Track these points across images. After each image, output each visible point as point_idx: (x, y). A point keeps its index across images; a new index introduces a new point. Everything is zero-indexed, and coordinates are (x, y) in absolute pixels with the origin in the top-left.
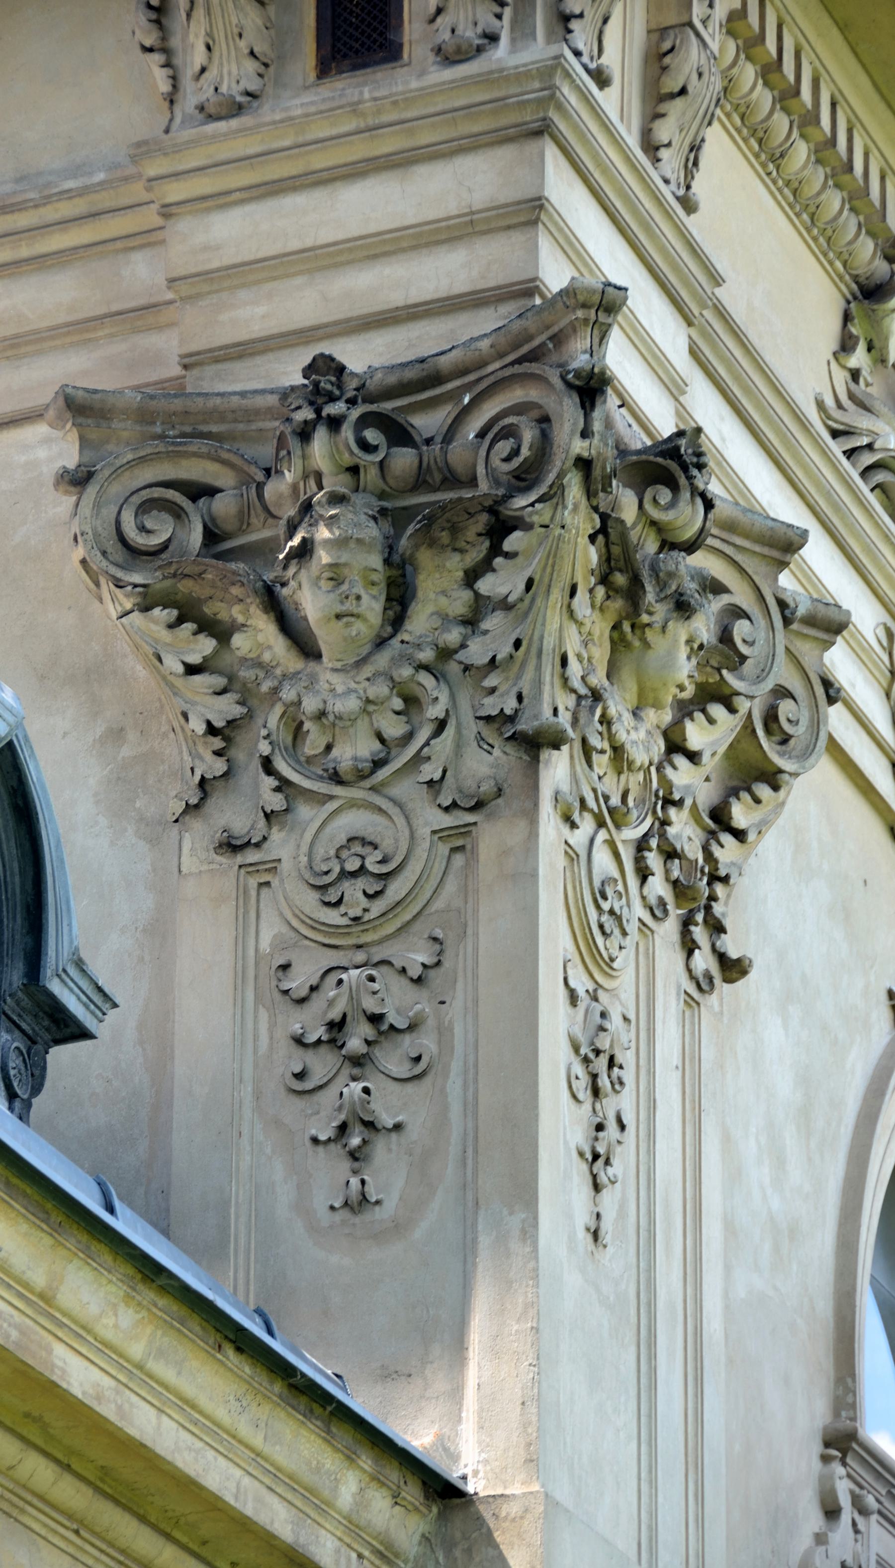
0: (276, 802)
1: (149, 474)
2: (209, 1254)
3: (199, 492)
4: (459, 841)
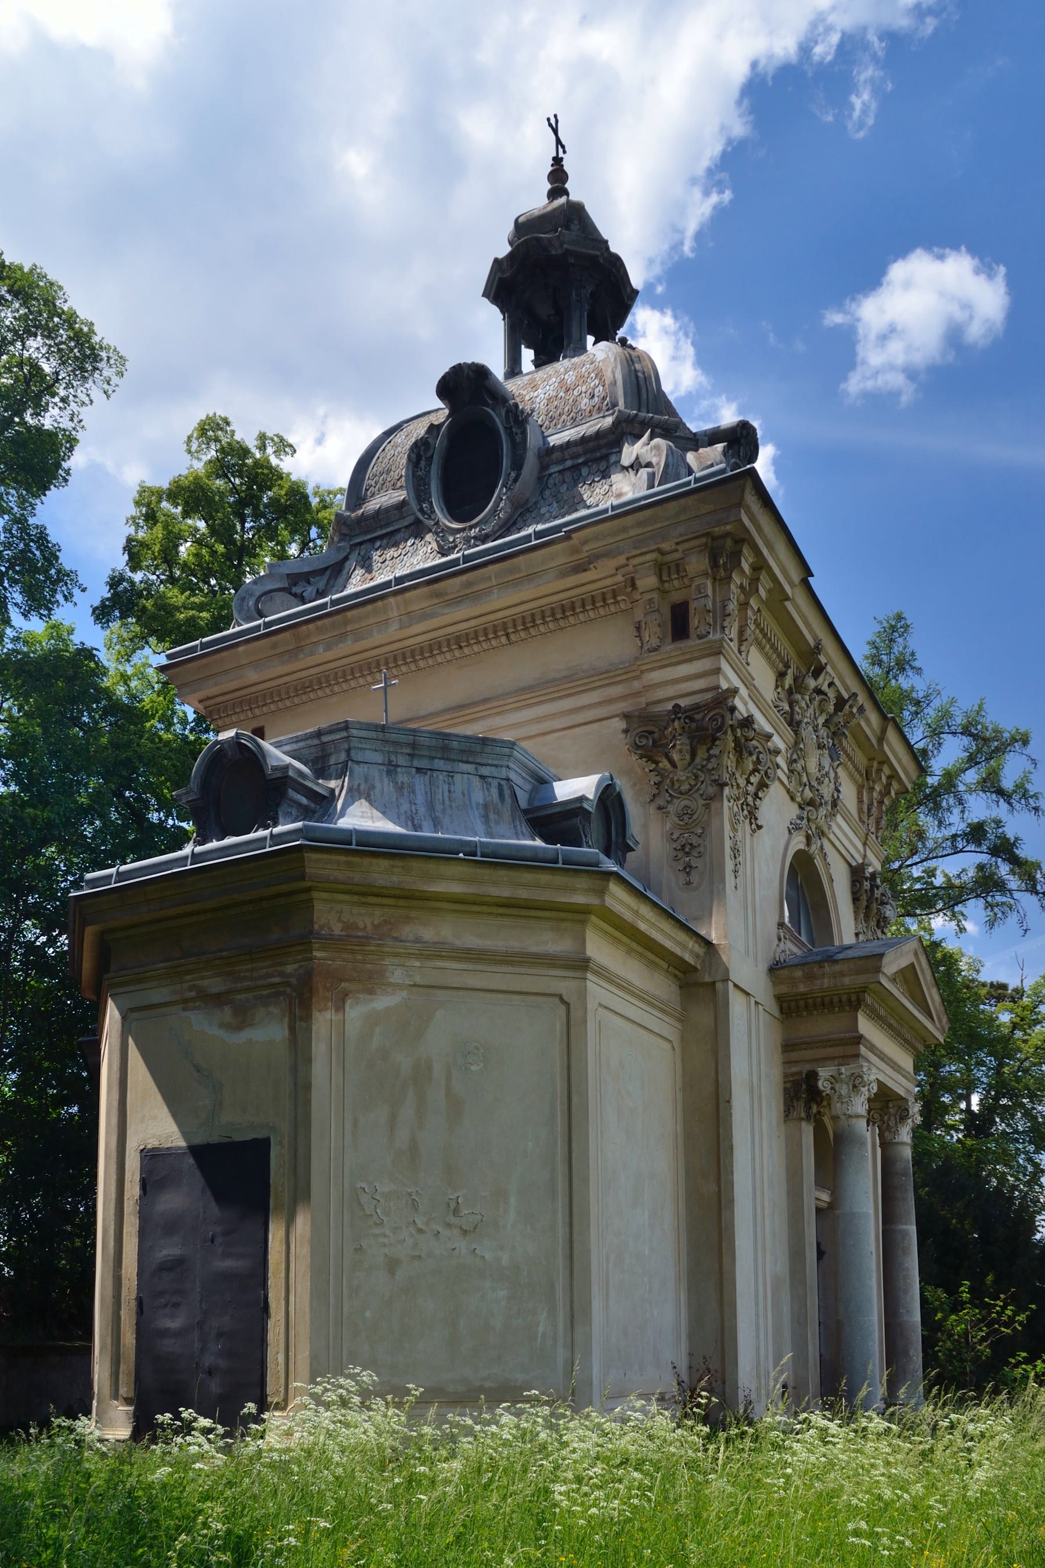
0: (669, 799)
1: (640, 730)
2: (659, 895)
3: (651, 733)
4: (707, 806)
